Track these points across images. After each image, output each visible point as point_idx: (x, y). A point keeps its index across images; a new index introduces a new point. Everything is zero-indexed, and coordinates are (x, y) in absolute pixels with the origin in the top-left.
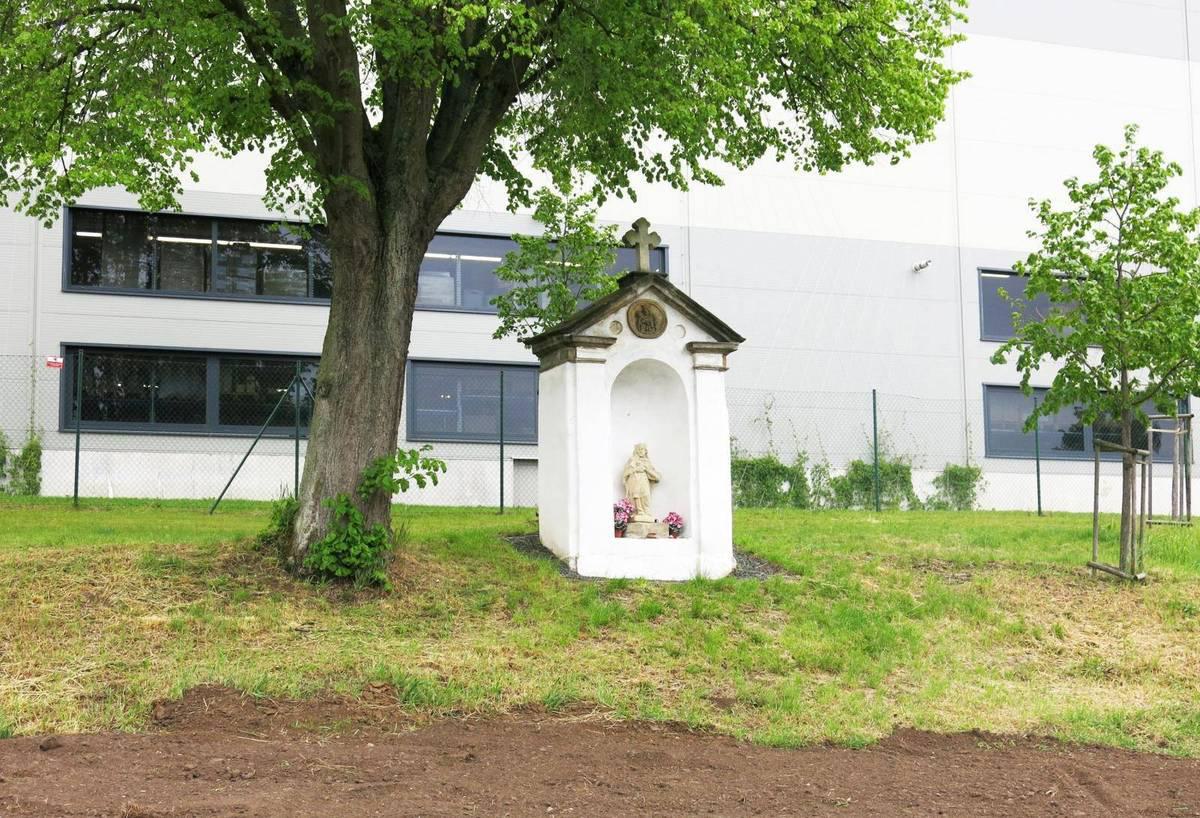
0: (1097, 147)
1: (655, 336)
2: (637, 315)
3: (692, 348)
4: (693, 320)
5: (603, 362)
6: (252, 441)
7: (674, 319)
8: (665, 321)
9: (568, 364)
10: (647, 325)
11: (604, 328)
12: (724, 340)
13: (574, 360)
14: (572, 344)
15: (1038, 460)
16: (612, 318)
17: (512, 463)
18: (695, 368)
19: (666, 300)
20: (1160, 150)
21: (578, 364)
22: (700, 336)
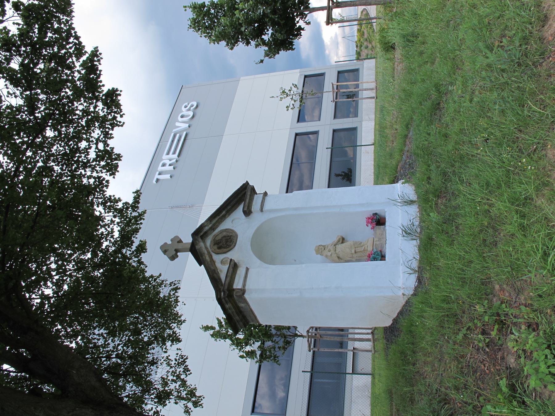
2: (219, 248)
3: (248, 212)
5: (247, 269)
7: (227, 224)
8: (226, 230)
9: (246, 296)
13: (243, 291)
18: (262, 210)
19: (213, 229)
21: (247, 288)
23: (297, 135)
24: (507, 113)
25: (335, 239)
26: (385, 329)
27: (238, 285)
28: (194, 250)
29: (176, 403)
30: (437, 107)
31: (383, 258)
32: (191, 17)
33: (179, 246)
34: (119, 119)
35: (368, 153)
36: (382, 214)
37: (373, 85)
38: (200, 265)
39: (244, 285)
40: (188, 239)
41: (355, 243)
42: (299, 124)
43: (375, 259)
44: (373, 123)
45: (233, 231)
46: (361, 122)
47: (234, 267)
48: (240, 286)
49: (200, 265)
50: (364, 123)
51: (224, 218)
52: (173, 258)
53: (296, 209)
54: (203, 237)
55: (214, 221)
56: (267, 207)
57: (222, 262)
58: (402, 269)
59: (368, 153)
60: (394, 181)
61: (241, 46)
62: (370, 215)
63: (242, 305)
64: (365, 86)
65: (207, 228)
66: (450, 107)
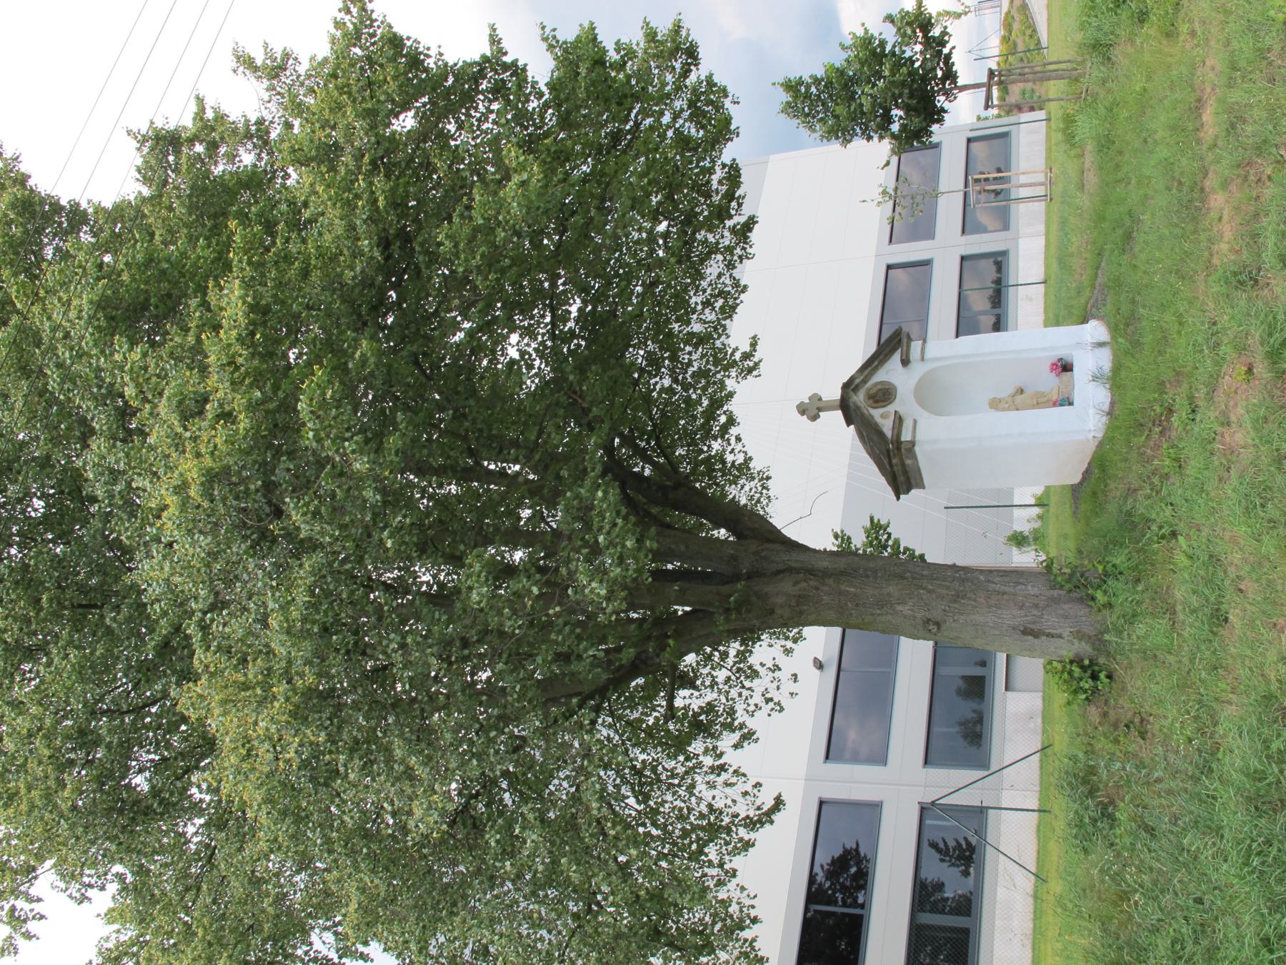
0: (745, 287)
1: (895, 389)
2: (876, 402)
3: (905, 362)
4: (882, 363)
5: (915, 422)
6: (988, 847)
7: (881, 376)
8: (881, 383)
9: (917, 449)
10: (884, 395)
11: (887, 427)
12: (900, 340)
13: (913, 443)
14: (898, 442)
15: (1039, 811)
16: (878, 420)
17: (1009, 694)
18: (923, 359)
19: (865, 381)
20: (811, 663)
21: (918, 438)
22: (896, 357)
23: (889, 267)
24: (288, 470)
25: (1011, 390)
26: (1075, 489)
27: (906, 436)
28: (846, 407)
29: (771, 646)
30: (1128, 237)
31: (1071, 404)
32: (785, 100)
33: (820, 404)
34: (749, 250)
35: (1031, 299)
36: (1069, 360)
37: (1040, 178)
38: (848, 425)
39: (914, 436)
40: (836, 394)
41: (1037, 393)
42: (892, 246)
43: (1061, 405)
44: (1040, 242)
45: (889, 383)
46: (1016, 239)
47: (899, 420)
48: (909, 438)
49: (848, 425)
50: (1021, 241)
51: (876, 369)
52: (814, 418)
53: (964, 356)
54: (856, 389)
55: (866, 372)
56: (928, 355)
57: (883, 416)
58: (1092, 411)
59: (1031, 299)
60: (1084, 321)
61: (858, 143)
62: (1055, 360)
63: (908, 462)
64: (1023, 179)
65: (857, 381)
66: (1140, 238)
